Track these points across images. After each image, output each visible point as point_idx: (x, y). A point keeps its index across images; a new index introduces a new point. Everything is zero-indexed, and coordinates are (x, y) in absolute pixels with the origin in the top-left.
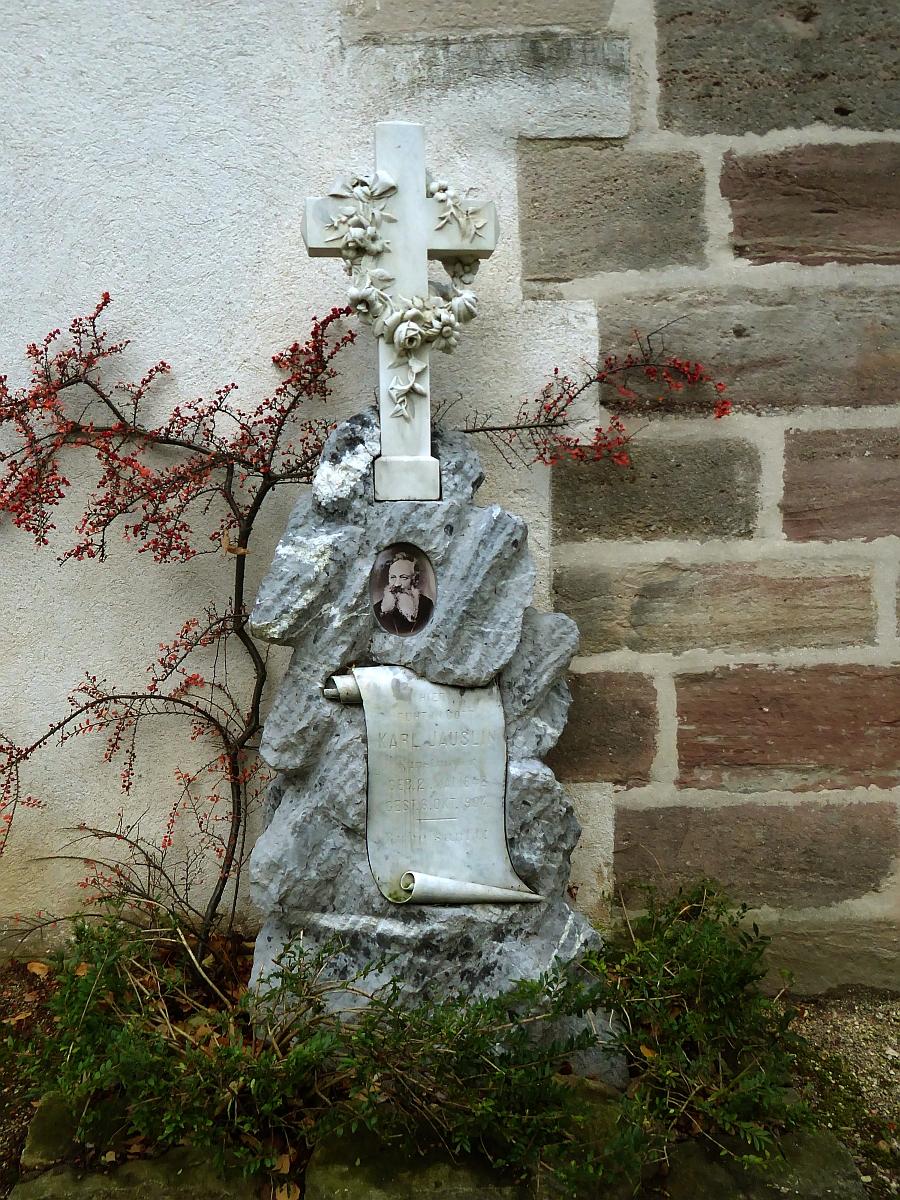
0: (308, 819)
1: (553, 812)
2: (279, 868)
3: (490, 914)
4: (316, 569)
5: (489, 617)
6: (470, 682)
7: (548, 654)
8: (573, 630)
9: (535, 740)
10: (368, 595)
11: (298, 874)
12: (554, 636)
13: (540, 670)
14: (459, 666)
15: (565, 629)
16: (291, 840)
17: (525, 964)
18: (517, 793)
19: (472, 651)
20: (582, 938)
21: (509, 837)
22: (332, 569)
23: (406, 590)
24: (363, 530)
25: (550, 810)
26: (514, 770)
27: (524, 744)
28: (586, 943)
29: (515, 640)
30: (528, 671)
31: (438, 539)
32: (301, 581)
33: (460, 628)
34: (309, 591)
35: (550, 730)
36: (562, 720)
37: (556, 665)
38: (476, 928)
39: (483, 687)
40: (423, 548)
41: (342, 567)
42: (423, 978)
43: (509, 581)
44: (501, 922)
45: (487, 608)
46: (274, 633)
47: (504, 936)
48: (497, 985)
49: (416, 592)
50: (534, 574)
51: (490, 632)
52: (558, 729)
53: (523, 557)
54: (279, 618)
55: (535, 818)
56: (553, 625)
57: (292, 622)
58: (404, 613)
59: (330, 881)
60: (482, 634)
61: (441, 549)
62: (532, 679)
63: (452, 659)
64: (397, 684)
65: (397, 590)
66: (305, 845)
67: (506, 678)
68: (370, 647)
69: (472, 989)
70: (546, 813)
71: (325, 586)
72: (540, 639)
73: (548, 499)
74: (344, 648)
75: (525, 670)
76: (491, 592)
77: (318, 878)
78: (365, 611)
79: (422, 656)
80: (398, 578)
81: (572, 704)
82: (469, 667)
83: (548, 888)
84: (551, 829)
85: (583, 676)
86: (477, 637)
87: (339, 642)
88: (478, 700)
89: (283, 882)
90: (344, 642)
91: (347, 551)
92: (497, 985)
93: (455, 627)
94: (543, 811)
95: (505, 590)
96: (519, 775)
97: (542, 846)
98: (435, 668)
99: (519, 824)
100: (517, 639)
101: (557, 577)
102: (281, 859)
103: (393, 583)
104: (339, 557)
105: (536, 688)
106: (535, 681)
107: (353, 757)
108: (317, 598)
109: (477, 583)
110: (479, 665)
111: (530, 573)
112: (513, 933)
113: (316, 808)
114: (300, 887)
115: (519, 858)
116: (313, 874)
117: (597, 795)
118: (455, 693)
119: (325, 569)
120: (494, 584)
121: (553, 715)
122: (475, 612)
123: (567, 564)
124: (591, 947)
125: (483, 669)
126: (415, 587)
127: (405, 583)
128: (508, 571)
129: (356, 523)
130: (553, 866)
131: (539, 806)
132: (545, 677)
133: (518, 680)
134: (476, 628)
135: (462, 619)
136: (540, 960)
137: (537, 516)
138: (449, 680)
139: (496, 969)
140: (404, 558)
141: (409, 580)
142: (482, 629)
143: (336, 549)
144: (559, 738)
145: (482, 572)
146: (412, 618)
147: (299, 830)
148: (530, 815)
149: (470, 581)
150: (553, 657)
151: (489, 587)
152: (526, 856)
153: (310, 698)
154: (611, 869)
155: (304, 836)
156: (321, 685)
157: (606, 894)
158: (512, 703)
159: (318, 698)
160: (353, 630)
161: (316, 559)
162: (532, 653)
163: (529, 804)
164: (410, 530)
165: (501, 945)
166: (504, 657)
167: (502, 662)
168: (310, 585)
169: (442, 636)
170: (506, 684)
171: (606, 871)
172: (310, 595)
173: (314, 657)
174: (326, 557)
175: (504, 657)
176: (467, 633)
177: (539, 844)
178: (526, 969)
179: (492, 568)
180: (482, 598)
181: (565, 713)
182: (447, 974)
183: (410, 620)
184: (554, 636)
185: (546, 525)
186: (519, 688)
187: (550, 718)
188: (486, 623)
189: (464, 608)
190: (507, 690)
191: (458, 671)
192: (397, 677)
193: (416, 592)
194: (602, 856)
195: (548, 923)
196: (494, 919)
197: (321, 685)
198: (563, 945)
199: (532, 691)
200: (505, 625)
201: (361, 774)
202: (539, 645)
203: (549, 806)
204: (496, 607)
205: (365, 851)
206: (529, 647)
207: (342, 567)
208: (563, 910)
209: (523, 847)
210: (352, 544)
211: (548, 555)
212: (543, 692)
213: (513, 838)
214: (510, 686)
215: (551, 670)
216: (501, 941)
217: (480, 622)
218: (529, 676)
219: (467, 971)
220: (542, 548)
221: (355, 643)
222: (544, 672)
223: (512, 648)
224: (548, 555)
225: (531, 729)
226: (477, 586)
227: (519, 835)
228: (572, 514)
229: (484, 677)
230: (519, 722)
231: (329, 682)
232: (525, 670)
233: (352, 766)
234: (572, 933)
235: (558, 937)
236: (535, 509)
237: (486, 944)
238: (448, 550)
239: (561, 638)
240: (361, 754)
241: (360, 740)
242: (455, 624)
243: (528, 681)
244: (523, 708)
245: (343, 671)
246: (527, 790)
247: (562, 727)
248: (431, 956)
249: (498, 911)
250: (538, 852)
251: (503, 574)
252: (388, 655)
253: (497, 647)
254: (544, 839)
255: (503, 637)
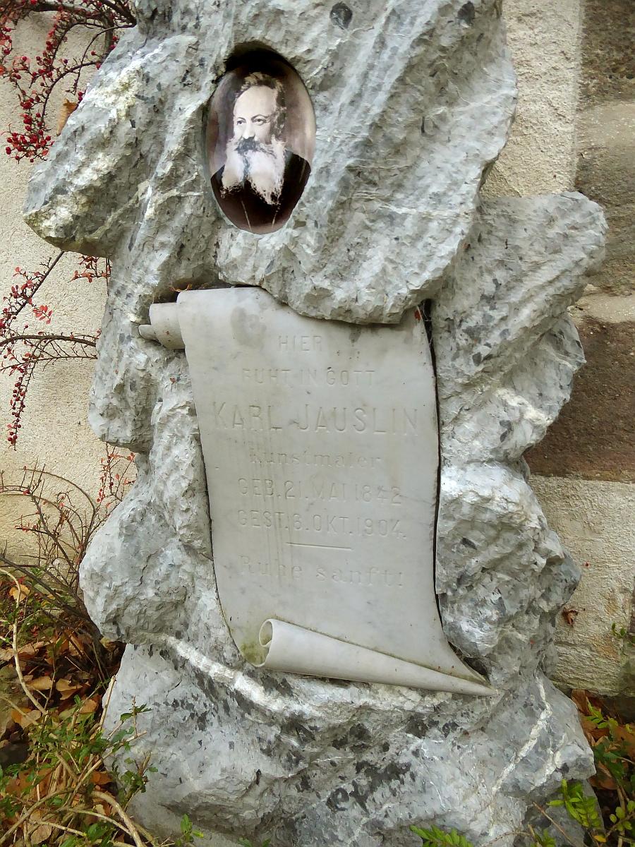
0: (138, 519)
1: (520, 564)
2: (103, 579)
3: (401, 699)
4: (113, 114)
5: (407, 184)
6: (361, 314)
7: (537, 266)
8: (594, 221)
9: (497, 430)
10: (196, 155)
11: (129, 592)
12: (552, 233)
13: (515, 298)
14: (344, 284)
15: (577, 218)
16: (118, 544)
17: (450, 790)
18: (451, 524)
19: (369, 253)
20: (559, 760)
21: (439, 591)
22: (141, 114)
23: (262, 145)
24: (192, 39)
25: (514, 558)
26: (450, 486)
27: (476, 436)
28: (565, 769)
29: (458, 230)
30: (490, 300)
31: (315, 31)
32: (87, 137)
33: (341, 205)
34: (100, 155)
35: (532, 413)
36: (560, 395)
37: (551, 290)
38: (375, 717)
39: (391, 326)
40: (284, 51)
41: (157, 111)
42: (297, 762)
43: (457, 109)
44: (420, 710)
45: (403, 164)
46: (49, 229)
47: (425, 728)
48: (406, 799)
49: (278, 147)
50: (513, 93)
51: (405, 216)
52: (550, 409)
53: (492, 61)
54: (52, 201)
55: (484, 570)
56: (551, 210)
57: (77, 210)
58: (259, 189)
59: (176, 605)
60: (391, 218)
61: (320, 51)
62: (497, 315)
63: (330, 268)
64: (241, 317)
65: (248, 145)
66: (136, 553)
67: (443, 312)
68: (215, 257)
69: (372, 788)
70: (507, 563)
71: (129, 145)
72: (521, 237)
73: (577, 26)
74: (163, 256)
75: (483, 297)
76: (410, 126)
77: (157, 599)
78: (192, 186)
79: (277, 263)
80: (249, 121)
81: (583, 369)
82: (361, 285)
83: (506, 671)
84: (515, 588)
85: (613, 327)
86: (380, 224)
87: (157, 245)
88: (384, 351)
89: (110, 600)
90: (163, 245)
91: (164, 80)
92: (406, 799)
93: (330, 203)
94: (501, 560)
95: (445, 128)
96: (455, 494)
97: (495, 618)
98: (300, 288)
99: (455, 574)
100: (463, 227)
101: (583, 167)
102: (103, 569)
103: (241, 131)
104: (151, 92)
105: (505, 332)
106: (504, 319)
107: (178, 437)
108: (119, 168)
109: (376, 104)
110: (383, 277)
111: (506, 91)
112: (441, 726)
113: (149, 504)
114: (134, 608)
115: (454, 627)
116: (150, 593)
117: (619, 499)
118: (342, 336)
119: (128, 115)
120: (416, 108)
121: (541, 385)
122: (373, 171)
123: (603, 142)
124: (573, 774)
125: (389, 288)
126: (277, 137)
127: (260, 131)
128: (452, 87)
129: (184, 29)
130: (520, 636)
131: (494, 552)
132: (526, 313)
133: (465, 316)
134: (377, 205)
135: (345, 185)
136: (481, 776)
137: (555, 60)
138: (326, 310)
139: (408, 774)
140: (260, 83)
141: (268, 125)
142: (393, 208)
143: (147, 79)
144: (550, 428)
145: (389, 81)
146: (273, 197)
147: (128, 532)
148: (474, 563)
149: (364, 104)
150: (546, 274)
151: (404, 115)
152: (465, 626)
153: (122, 339)
154: (629, 597)
155: (134, 542)
156: (133, 318)
157: (618, 627)
158: (454, 359)
159: (129, 338)
160: (177, 223)
161: (113, 97)
162: (501, 263)
163: (473, 547)
164: (255, 11)
165: (419, 741)
166: (431, 266)
167: (427, 275)
168: (102, 144)
169: (310, 224)
170: (442, 324)
171: (621, 598)
172: (103, 163)
173: (128, 273)
174: (131, 93)
175: (431, 266)
176: (359, 217)
177: (489, 613)
178: (451, 799)
179: (410, 68)
180: (388, 140)
181: (566, 381)
182: (333, 763)
183: (269, 201)
184: (552, 233)
185: (570, 75)
186: (470, 332)
187: (535, 391)
188: (399, 196)
189: (350, 162)
190: (446, 334)
191: (340, 294)
192: (242, 305)
193: (278, 147)
194: (618, 580)
195: (504, 716)
196: (408, 706)
197: (133, 318)
198: (524, 760)
199: (495, 338)
200: (438, 198)
201: (185, 467)
202: (517, 248)
203: (511, 554)
204: (424, 164)
205: (210, 577)
206: (497, 252)
207: (157, 111)
208: (533, 699)
209: (461, 612)
210: (173, 66)
211: (570, 128)
212: (520, 341)
213: (444, 595)
214: (451, 325)
215: (541, 298)
216: (420, 735)
217: (387, 193)
218: (493, 308)
219: (366, 763)
220: (560, 116)
221: (182, 246)
222: (524, 302)
223: (451, 245)
224: (570, 128)
225: (491, 409)
226: (376, 110)
227: (454, 591)
228: (619, 49)
229: (390, 305)
230: (466, 396)
231: (144, 316)
232: (483, 297)
233: (175, 452)
234: (542, 745)
235: (518, 745)
236: (553, 47)
237: (396, 736)
238: (335, 55)
239: (566, 236)
240: (188, 433)
241: (185, 411)
242: (333, 195)
243: (488, 318)
244: (474, 370)
245: (168, 296)
246: (471, 523)
247: (558, 407)
248: (305, 740)
249: (414, 696)
250: (487, 626)
251: (441, 89)
252: (235, 267)
253: (420, 245)
254: (500, 605)
255: (434, 225)
